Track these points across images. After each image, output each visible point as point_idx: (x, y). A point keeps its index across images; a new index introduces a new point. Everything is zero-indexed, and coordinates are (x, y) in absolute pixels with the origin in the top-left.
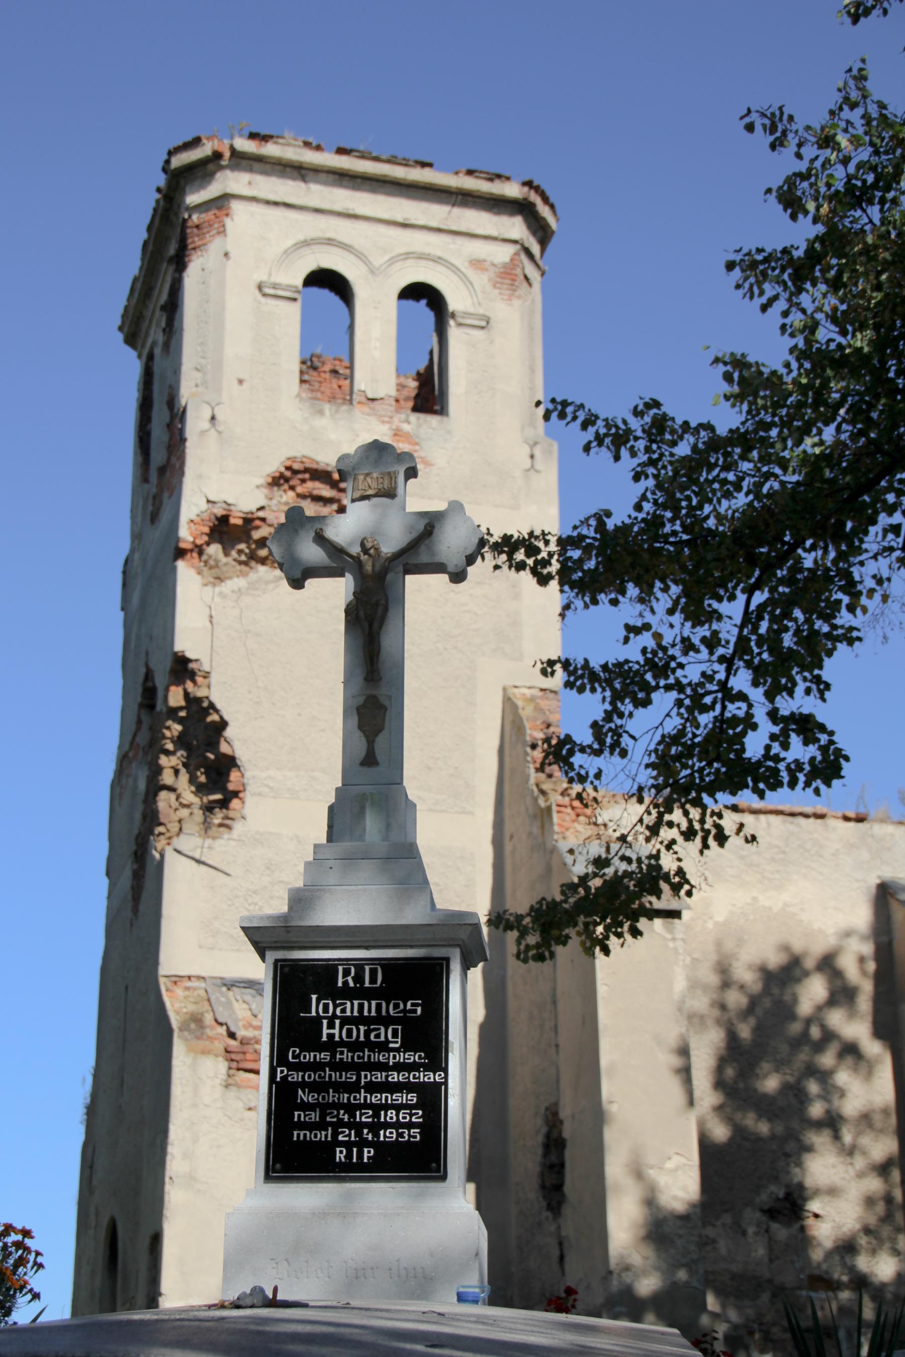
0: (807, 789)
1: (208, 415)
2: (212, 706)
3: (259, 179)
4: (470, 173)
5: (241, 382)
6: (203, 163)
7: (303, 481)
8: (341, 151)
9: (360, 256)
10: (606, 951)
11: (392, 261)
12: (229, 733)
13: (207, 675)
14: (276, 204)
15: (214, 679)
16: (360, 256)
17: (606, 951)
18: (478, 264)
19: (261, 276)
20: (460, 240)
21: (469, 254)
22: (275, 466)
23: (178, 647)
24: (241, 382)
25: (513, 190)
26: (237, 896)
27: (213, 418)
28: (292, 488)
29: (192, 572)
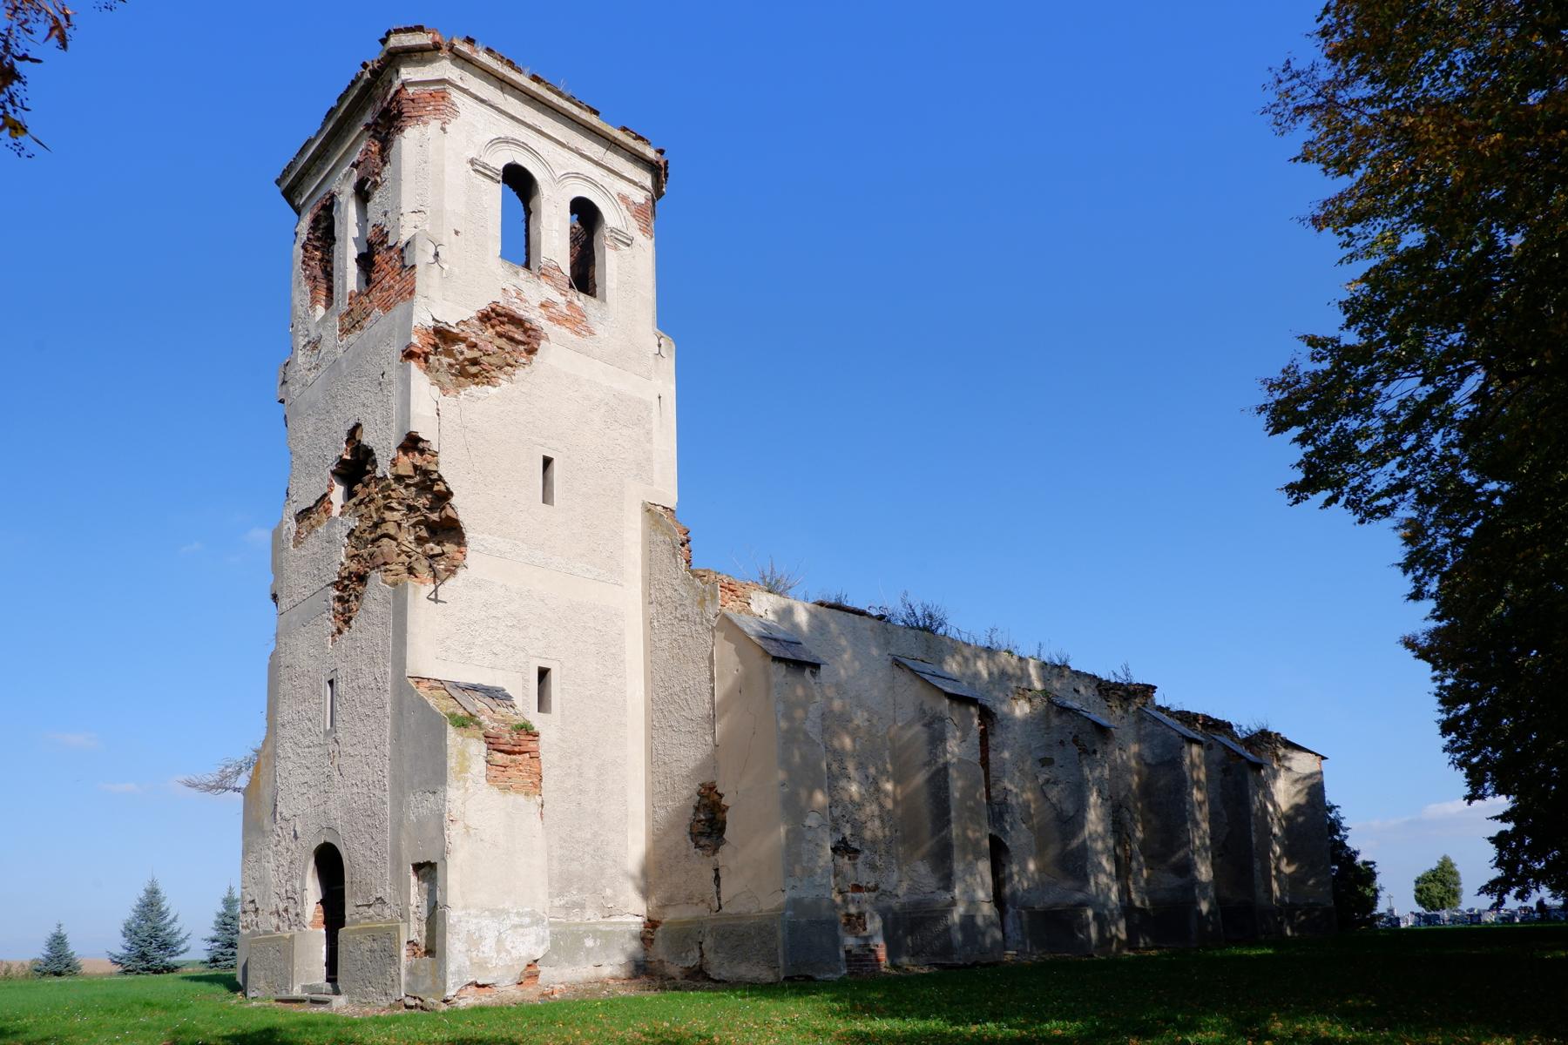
0: (1297, 444)
1: (432, 252)
2: (440, 478)
3: (467, 76)
4: (624, 129)
5: (457, 233)
6: (422, 49)
7: (502, 323)
8: (535, 79)
9: (545, 163)
10: (1435, 679)
11: (567, 175)
12: (453, 501)
13: (435, 454)
14: (482, 101)
15: (441, 458)
16: (545, 163)
17: (1435, 679)
18: (624, 198)
19: (472, 154)
20: (612, 176)
21: (619, 191)
22: (484, 305)
23: (605, 965)
24: (457, 233)
25: (650, 153)
26: (523, 649)
27: (437, 255)
28: (493, 326)
29: (421, 373)
